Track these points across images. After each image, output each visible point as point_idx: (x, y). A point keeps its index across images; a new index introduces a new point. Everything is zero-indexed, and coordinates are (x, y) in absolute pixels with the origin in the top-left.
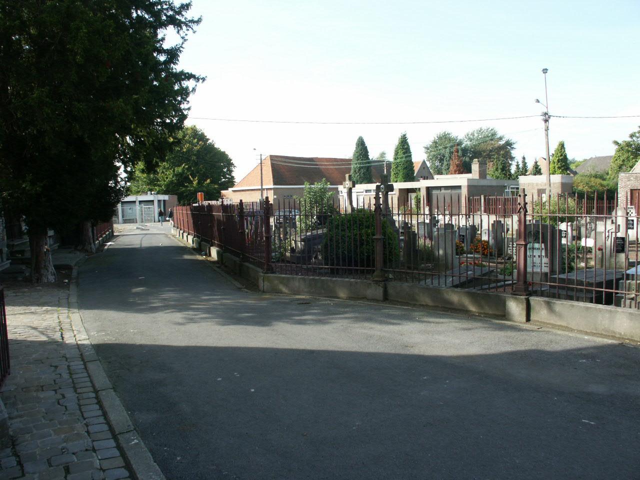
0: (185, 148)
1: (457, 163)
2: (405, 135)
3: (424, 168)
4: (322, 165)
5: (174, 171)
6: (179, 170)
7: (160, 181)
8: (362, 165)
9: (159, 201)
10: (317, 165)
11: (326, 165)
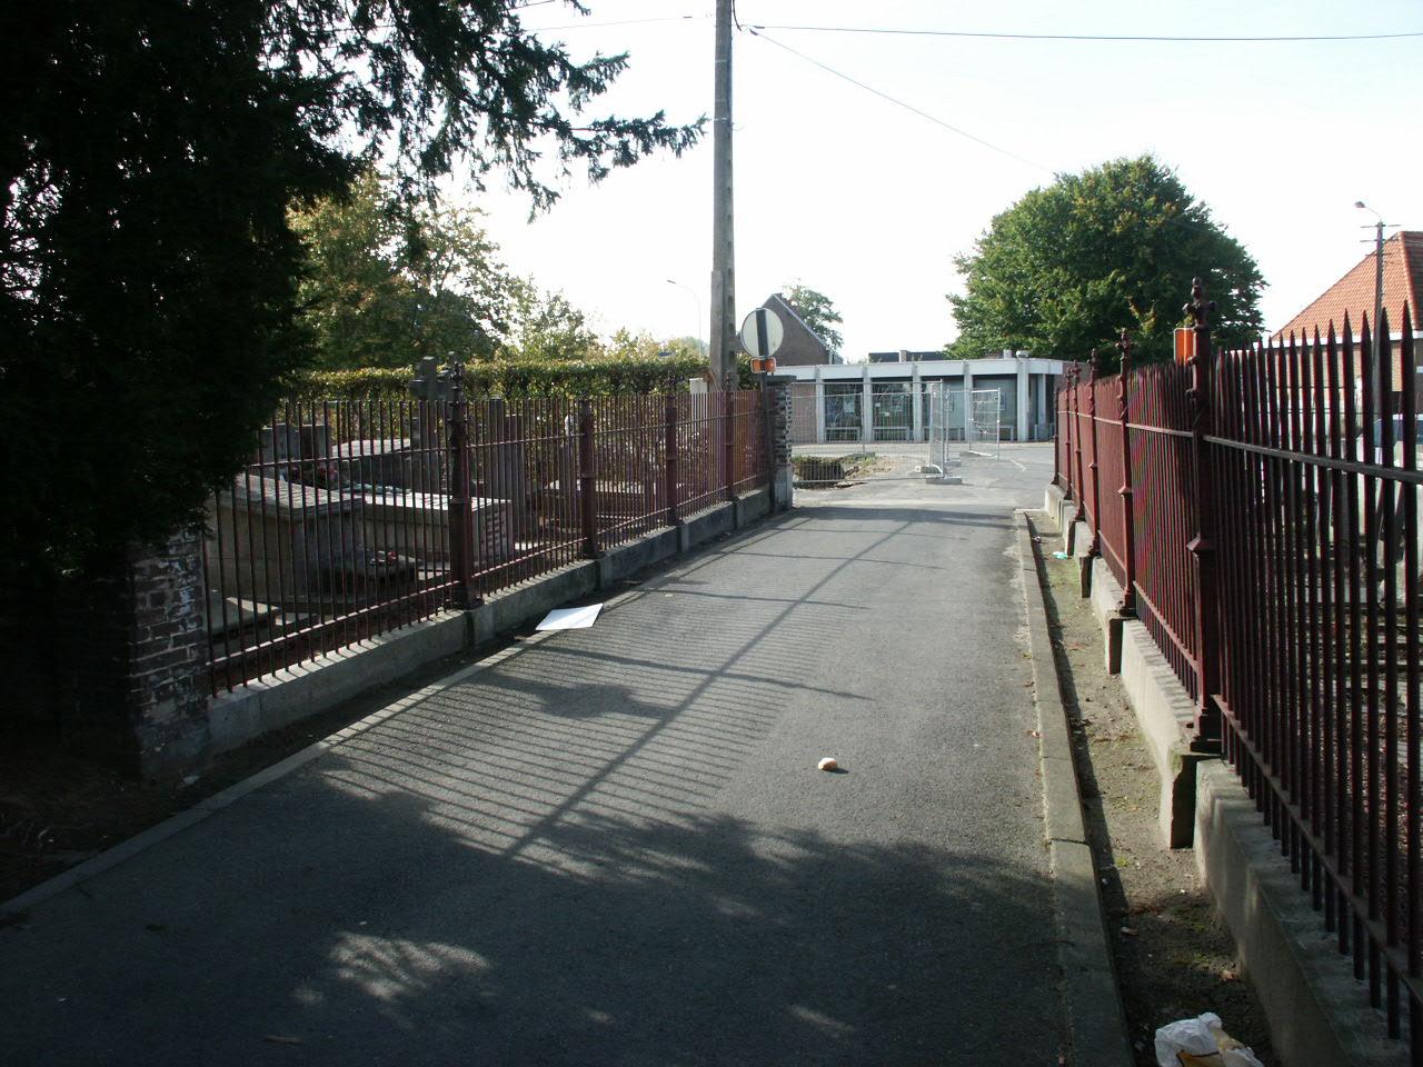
5: (1083, 292)
6: (1101, 287)
7: (1041, 321)
9: (1034, 378)
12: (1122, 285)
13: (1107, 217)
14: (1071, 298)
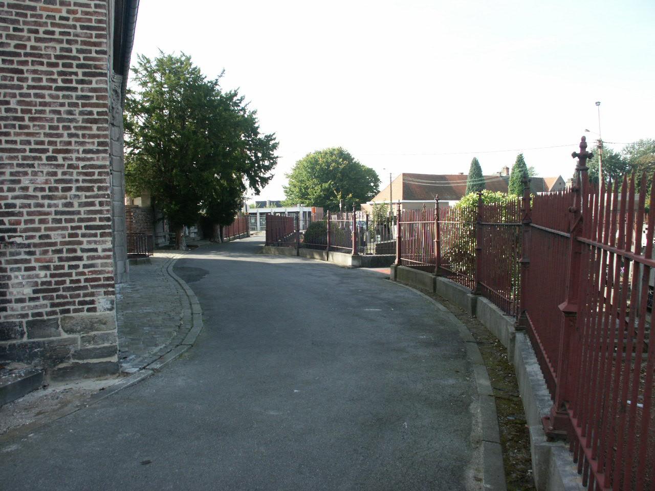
2: (521, 155)
3: (560, 183)
4: (453, 183)
5: (321, 186)
6: (326, 185)
7: (309, 195)
8: (475, 183)
9: (304, 213)
10: (449, 183)
12: (333, 185)
13: (328, 165)
14: (318, 188)
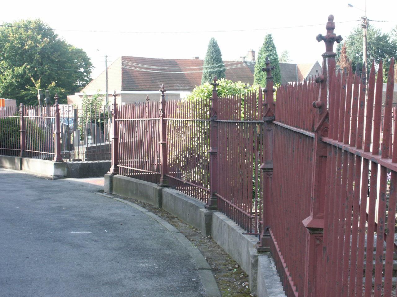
0: (27, 45)
1: (345, 66)
2: (270, 35)
4: (186, 70)
5: (13, 71)
6: (19, 70)
8: (212, 70)
11: (192, 70)
